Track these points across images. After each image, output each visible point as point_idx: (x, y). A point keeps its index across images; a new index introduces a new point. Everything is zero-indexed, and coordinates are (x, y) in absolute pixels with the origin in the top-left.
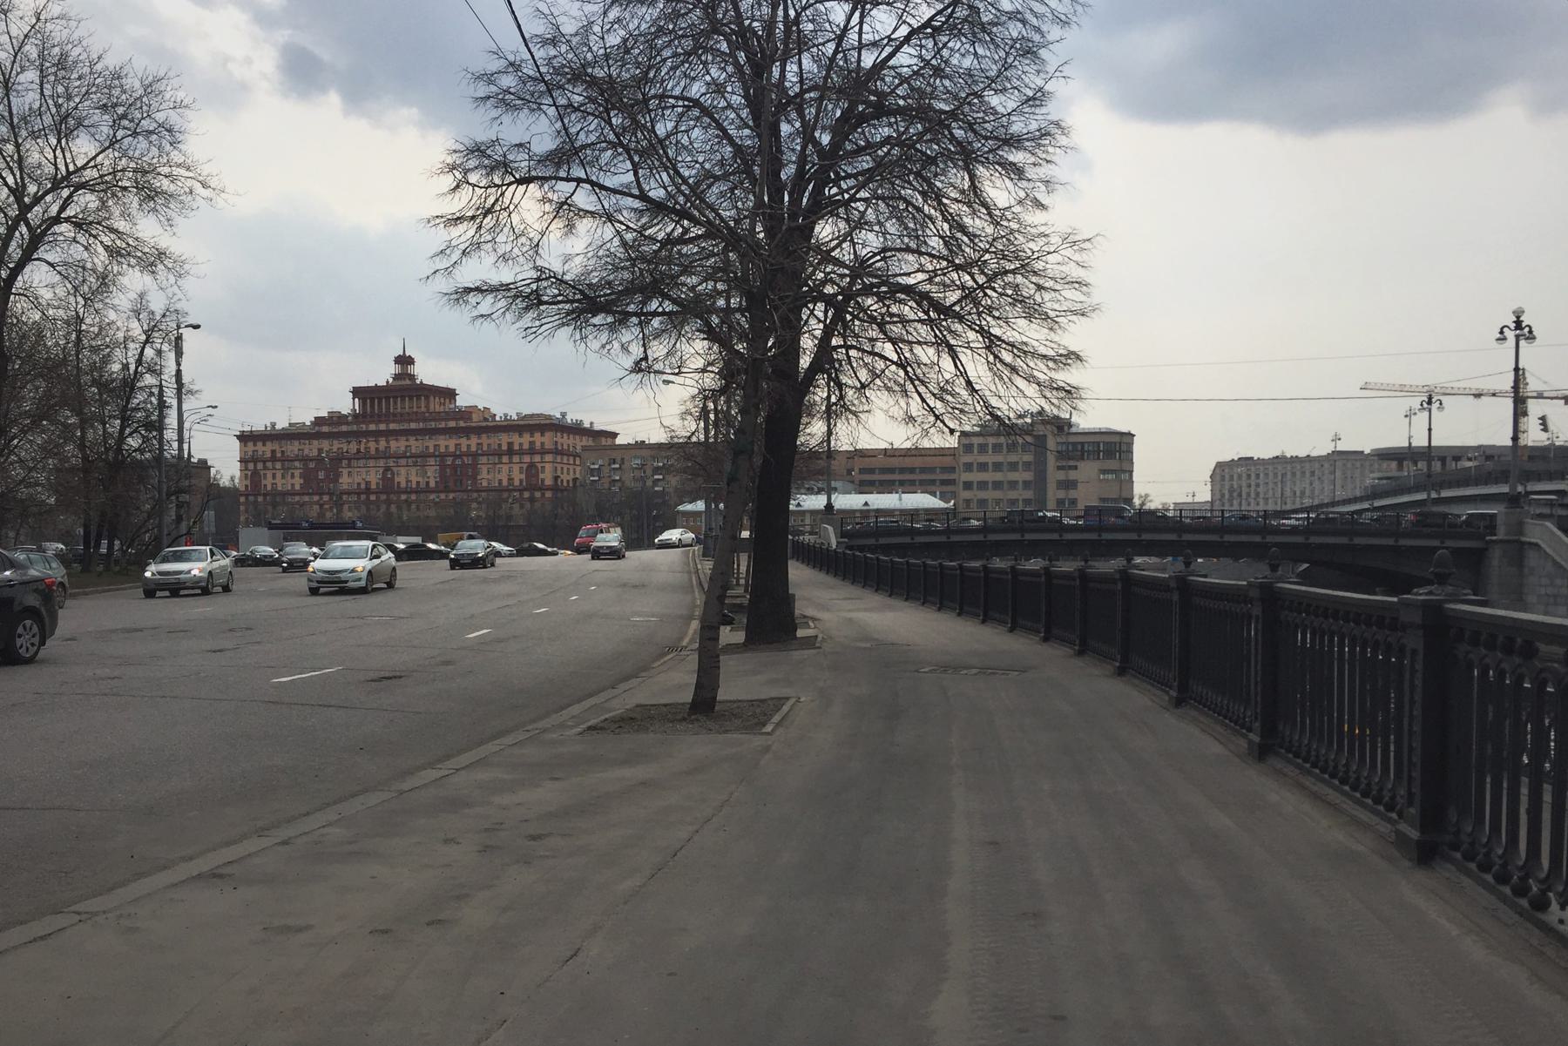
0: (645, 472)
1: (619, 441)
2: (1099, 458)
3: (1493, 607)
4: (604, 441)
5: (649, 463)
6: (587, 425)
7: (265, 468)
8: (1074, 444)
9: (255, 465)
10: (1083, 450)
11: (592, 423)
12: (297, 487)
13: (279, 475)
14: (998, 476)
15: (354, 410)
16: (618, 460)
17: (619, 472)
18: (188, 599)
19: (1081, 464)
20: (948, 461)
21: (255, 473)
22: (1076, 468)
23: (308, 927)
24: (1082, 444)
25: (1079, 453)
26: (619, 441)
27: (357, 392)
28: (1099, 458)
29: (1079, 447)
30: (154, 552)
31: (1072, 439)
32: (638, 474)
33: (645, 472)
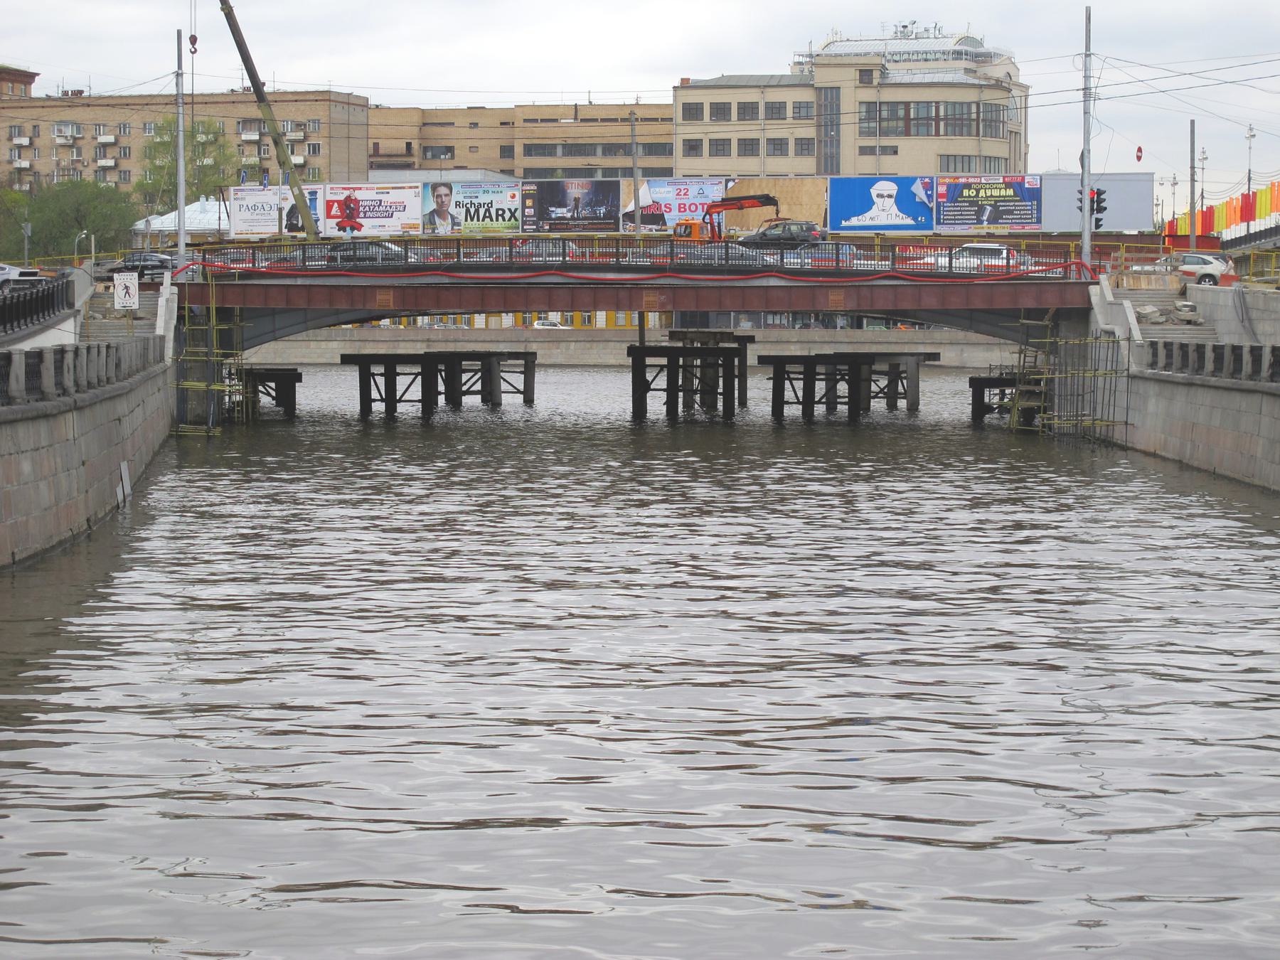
0: (79, 154)
1: (37, 90)
2: (937, 134)
3: (16, 660)
5: (88, 136)
8: (893, 105)
10: (907, 118)
14: (749, 130)
16: (28, 127)
17: (30, 153)
18: (780, 89)
19: (902, 143)
20: (647, 133)
22: (895, 151)
23: (64, 854)
24: (907, 104)
25: (901, 124)
26: (37, 90)
28: (937, 134)
29: (901, 113)
31: (889, 95)
32: (67, 158)
33: (79, 154)
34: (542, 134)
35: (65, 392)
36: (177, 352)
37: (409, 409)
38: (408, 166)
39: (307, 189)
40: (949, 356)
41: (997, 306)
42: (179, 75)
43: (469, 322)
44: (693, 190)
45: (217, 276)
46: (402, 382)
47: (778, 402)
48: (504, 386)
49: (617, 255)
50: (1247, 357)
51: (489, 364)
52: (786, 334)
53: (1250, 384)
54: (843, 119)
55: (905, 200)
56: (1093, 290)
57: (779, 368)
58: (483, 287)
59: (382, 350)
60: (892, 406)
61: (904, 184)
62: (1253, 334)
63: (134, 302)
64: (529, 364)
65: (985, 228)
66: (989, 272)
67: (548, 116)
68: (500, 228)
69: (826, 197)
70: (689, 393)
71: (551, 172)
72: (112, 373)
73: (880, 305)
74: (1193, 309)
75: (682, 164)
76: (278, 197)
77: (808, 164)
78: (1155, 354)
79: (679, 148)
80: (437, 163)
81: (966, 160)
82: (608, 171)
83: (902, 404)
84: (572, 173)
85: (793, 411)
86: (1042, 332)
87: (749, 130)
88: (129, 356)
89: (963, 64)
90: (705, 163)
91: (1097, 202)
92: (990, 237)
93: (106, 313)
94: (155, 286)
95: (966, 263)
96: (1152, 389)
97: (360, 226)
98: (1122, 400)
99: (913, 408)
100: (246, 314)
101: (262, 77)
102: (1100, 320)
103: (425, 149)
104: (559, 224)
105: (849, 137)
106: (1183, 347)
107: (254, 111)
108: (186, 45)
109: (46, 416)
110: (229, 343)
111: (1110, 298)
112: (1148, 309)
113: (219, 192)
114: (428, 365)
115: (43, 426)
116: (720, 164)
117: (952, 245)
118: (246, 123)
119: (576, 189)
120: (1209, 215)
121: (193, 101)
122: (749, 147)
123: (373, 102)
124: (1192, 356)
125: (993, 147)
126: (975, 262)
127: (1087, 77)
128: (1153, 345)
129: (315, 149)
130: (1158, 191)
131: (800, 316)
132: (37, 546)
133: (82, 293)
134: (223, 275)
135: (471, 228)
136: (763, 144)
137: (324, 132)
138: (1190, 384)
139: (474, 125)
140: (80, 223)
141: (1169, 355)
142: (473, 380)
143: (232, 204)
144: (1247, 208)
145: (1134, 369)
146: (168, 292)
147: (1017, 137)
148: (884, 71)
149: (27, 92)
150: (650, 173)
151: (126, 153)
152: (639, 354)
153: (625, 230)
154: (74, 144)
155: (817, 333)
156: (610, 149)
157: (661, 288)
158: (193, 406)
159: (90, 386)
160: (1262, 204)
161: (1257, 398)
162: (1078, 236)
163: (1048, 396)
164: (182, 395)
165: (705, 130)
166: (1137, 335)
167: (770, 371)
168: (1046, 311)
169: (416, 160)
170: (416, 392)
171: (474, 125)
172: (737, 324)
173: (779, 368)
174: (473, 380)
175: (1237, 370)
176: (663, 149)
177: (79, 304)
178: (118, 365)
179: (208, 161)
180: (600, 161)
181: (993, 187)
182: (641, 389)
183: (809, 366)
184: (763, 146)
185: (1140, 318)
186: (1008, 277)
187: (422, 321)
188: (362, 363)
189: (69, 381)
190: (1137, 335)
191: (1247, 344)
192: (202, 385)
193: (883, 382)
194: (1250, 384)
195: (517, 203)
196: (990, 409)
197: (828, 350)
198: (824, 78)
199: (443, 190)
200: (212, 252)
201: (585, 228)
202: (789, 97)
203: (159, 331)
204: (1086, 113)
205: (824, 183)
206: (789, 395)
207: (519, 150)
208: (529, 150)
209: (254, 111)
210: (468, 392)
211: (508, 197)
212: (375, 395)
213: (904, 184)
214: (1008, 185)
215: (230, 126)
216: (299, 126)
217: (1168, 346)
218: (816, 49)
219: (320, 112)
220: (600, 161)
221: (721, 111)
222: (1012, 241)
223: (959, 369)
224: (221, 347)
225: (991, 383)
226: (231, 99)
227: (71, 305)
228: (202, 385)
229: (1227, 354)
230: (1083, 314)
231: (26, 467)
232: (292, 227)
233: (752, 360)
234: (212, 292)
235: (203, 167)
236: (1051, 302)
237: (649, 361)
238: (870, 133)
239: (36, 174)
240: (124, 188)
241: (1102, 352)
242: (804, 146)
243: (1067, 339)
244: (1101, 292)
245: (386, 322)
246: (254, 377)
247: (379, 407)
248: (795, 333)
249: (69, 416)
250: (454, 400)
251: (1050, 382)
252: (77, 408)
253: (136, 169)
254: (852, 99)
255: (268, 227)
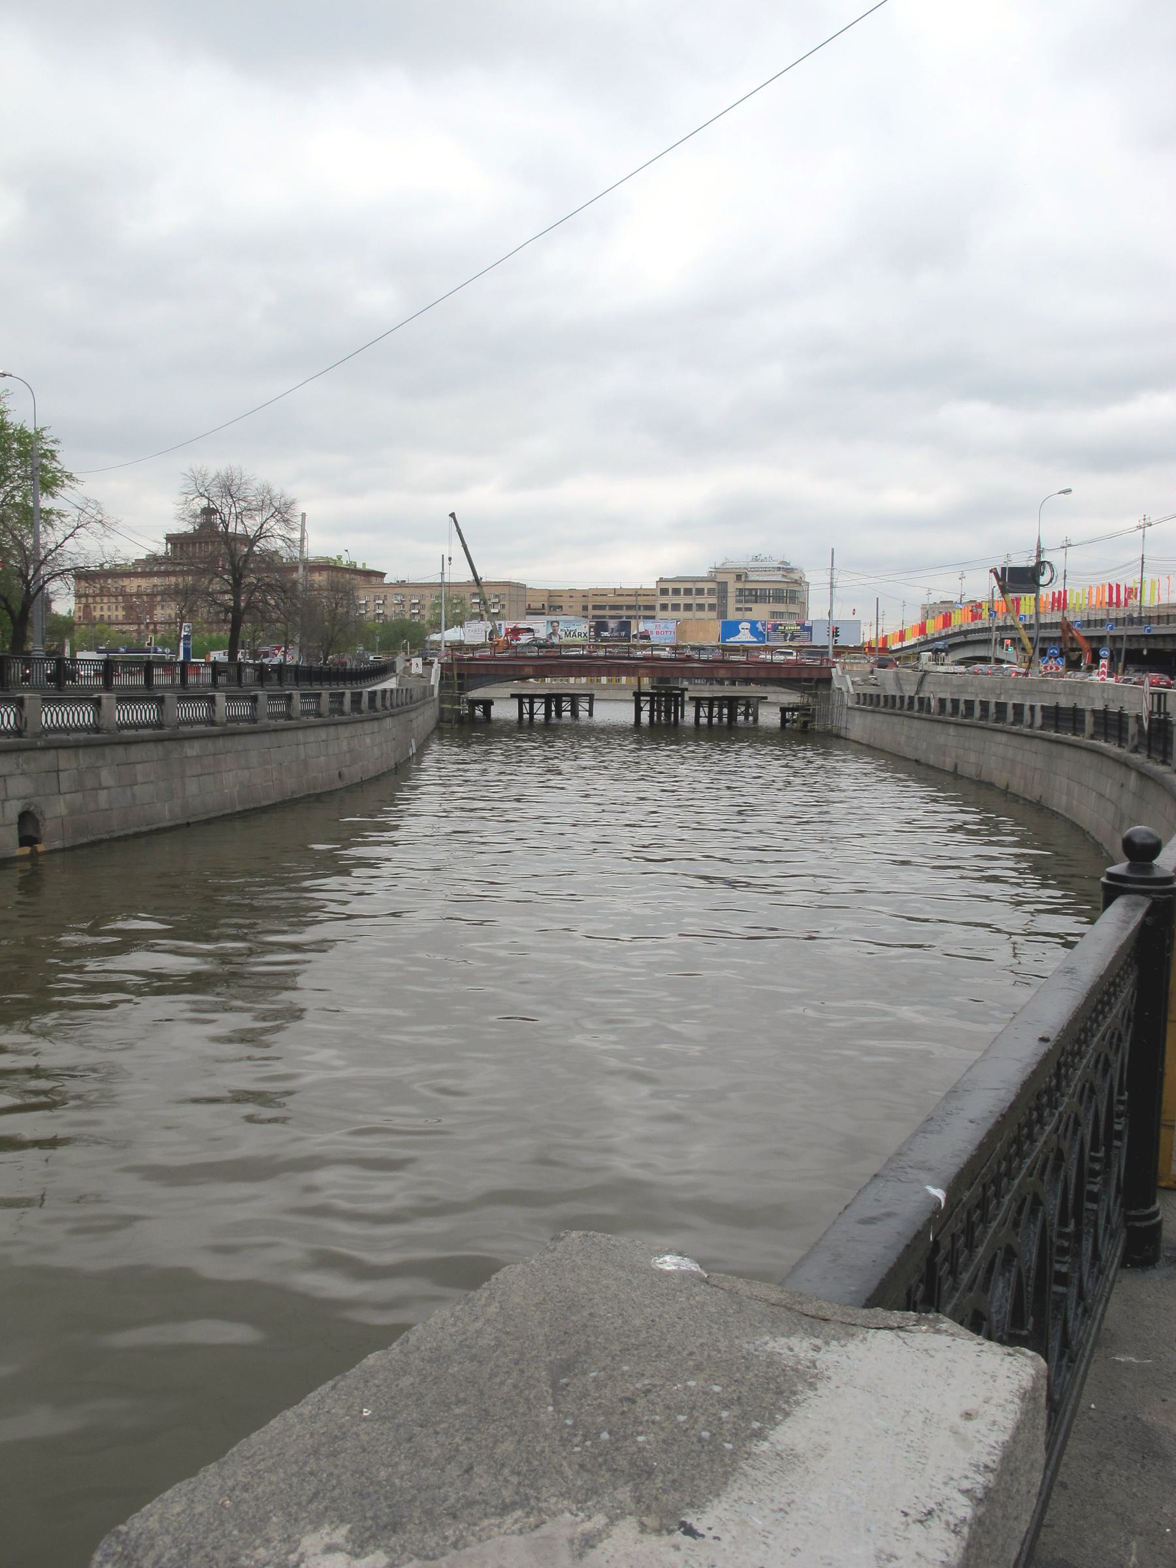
1: (386, 580)
4: (373, 579)
6: (360, 566)
7: (95, 602)
8: (751, 590)
9: (87, 600)
11: (364, 564)
12: (120, 618)
13: (105, 607)
14: (688, 600)
15: (167, 553)
16: (383, 598)
20: (642, 601)
21: (87, 606)
22: (750, 609)
26: (386, 580)
27: (170, 538)
29: (754, 593)
30: (111, 918)
31: (749, 586)
32: (398, 609)
34: (600, 601)
35: (386, 709)
36: (440, 692)
37: (540, 716)
38: (543, 614)
39: (497, 623)
40: (771, 698)
41: (791, 676)
42: (442, 574)
43: (567, 681)
44: (662, 625)
45: (457, 660)
46: (536, 706)
47: (697, 716)
48: (580, 708)
49: (629, 653)
50: (898, 700)
51: (574, 699)
52: (703, 687)
53: (899, 712)
54: (729, 595)
55: (753, 631)
56: (833, 670)
57: (698, 702)
58: (570, 666)
59: (530, 692)
60: (746, 718)
61: (753, 624)
62: (901, 690)
63: (420, 670)
64: (591, 699)
65: (788, 643)
66: (788, 662)
67: (602, 593)
68: (579, 640)
69: (720, 629)
70: (659, 712)
71: (604, 617)
72: (408, 700)
73: (743, 675)
74: (876, 679)
75: (659, 614)
76: (485, 626)
77: (714, 615)
78: (859, 698)
79: (658, 607)
80: (554, 613)
81: (781, 614)
82: (628, 617)
83: (751, 718)
84: (612, 617)
85: (703, 721)
86: (811, 688)
87: (688, 600)
88: (416, 694)
89: (782, 573)
90: (669, 614)
91: (836, 633)
92: (790, 647)
93: (410, 675)
94: (431, 663)
95: (779, 658)
96: (857, 713)
97: (519, 639)
98: (844, 718)
99: (756, 720)
100: (470, 676)
101: (479, 575)
102: (836, 683)
103: (550, 607)
104: (605, 639)
105: (732, 603)
106: (871, 695)
107: (476, 590)
108: (446, 561)
109: (377, 719)
110: (462, 688)
111: (840, 674)
112: (857, 679)
113: (461, 624)
114: (548, 699)
115: (376, 724)
116: (676, 614)
117: (772, 650)
118: (474, 595)
119: (612, 624)
120: (885, 639)
121: (450, 585)
122: (688, 607)
123: (528, 586)
124: (875, 700)
125: (793, 608)
126: (782, 657)
127: (832, 578)
128: (858, 694)
129: (503, 606)
130: (863, 628)
131: (710, 680)
132: (373, 774)
133: (399, 667)
134: (460, 659)
135: (566, 640)
136: (694, 606)
137: (507, 598)
138: (873, 712)
139: (571, 597)
140: (403, 636)
141: (865, 699)
142: (566, 705)
143: (466, 629)
144: (902, 636)
145: (850, 705)
146: (436, 667)
147: (804, 604)
148: (747, 576)
149: (382, 581)
150: (646, 617)
151: (423, 607)
152: (638, 695)
153: (633, 642)
154: (401, 603)
155: (716, 687)
156: (629, 607)
157: (647, 667)
158: (447, 715)
159: (398, 706)
160: (908, 634)
161: (902, 718)
162: (827, 647)
163: (813, 716)
164: (442, 710)
165: (670, 600)
166: (851, 690)
167: (694, 703)
168: (812, 679)
169: (546, 611)
170: (542, 710)
171: (571, 597)
172: (682, 682)
173: (698, 702)
174: (566, 705)
175: (893, 706)
176: (652, 608)
177: (398, 671)
178: (411, 697)
179: (458, 611)
180: (624, 613)
181: (791, 625)
182: (638, 710)
183: (711, 701)
184: (694, 607)
185: (853, 683)
186: (797, 665)
187: (548, 680)
188: (520, 697)
189: (388, 704)
190: (851, 690)
191: (898, 694)
192: (450, 706)
193: (743, 709)
194: (899, 712)
195: (587, 630)
196: (788, 721)
197: (720, 695)
198: (721, 578)
199: (555, 624)
200: (457, 649)
201: (616, 641)
202: (706, 586)
203: (432, 683)
204: (831, 594)
205: (719, 623)
206: (702, 714)
207: (590, 607)
208: (595, 607)
209: (476, 590)
210: (565, 711)
211: (583, 627)
212: (525, 711)
213: (753, 624)
214: (798, 625)
215: (468, 595)
216: (497, 596)
217: (865, 695)
218: (717, 566)
219: (506, 590)
220: (624, 613)
221: (676, 592)
222: (799, 649)
223: (774, 704)
224: (459, 690)
225: (793, 710)
226: (467, 584)
227: (395, 672)
228: (450, 706)
229: (890, 698)
230: (828, 681)
231: (368, 741)
232: (491, 639)
233: (686, 698)
234: (455, 667)
235: (455, 613)
236: (815, 675)
237: (642, 698)
238: (740, 602)
239: (386, 616)
240: (422, 622)
241: (836, 697)
242: (712, 607)
243: (822, 692)
244: (836, 672)
245: (531, 680)
246: (474, 703)
247: (526, 716)
248: (707, 688)
249: (388, 719)
250: (559, 715)
251: (814, 709)
252: (392, 715)
253: (428, 614)
254: (733, 587)
255: (480, 639)
